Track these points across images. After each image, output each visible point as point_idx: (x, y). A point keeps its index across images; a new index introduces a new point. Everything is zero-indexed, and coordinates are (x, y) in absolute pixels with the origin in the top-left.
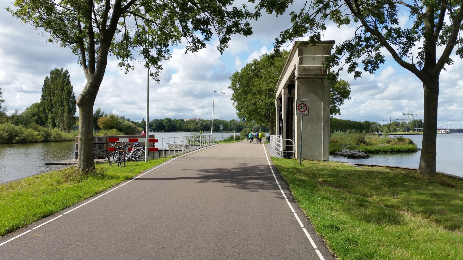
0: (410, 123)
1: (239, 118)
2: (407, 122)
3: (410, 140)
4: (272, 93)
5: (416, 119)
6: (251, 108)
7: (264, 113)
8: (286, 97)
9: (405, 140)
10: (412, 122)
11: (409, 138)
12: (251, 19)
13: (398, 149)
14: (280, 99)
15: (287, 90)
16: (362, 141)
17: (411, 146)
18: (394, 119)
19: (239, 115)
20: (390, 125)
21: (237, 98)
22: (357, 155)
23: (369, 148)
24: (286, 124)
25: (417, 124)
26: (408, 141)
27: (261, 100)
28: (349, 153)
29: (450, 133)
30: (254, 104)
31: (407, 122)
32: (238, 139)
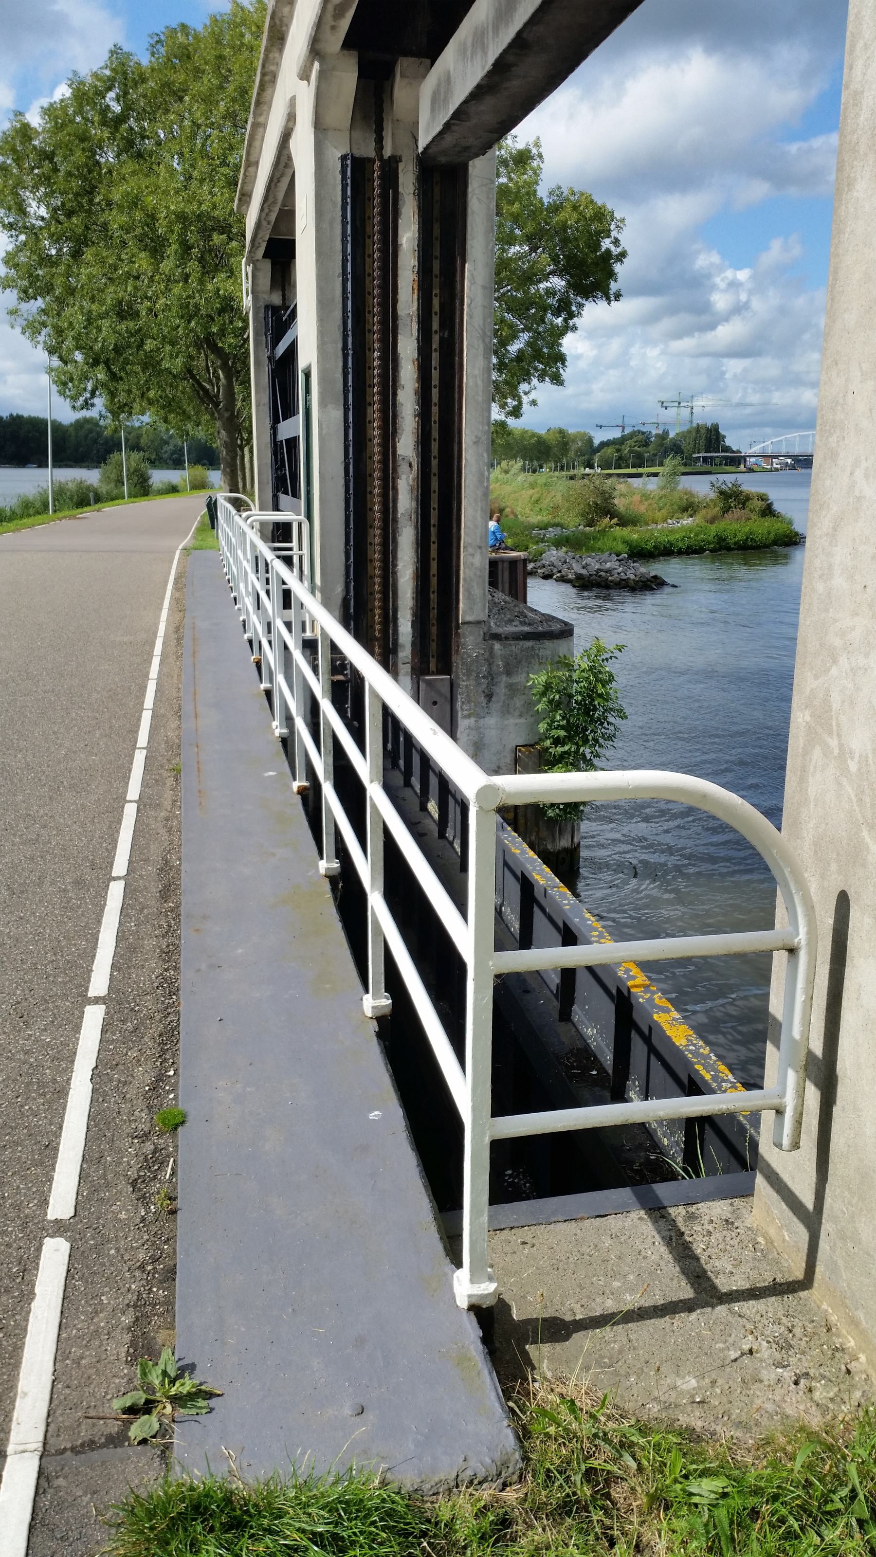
0: (683, 435)
1: (62, 393)
2: (672, 435)
3: (763, 498)
4: (217, 239)
5: (700, 422)
6: (107, 333)
7: (179, 361)
8: (334, 154)
9: (748, 498)
10: (689, 432)
11: (762, 490)
12: (147, 49)
13: (740, 537)
14: (280, 253)
15: (347, 79)
16: (603, 508)
17: (761, 528)
18: (634, 422)
19: (63, 383)
20: (621, 441)
21: (33, 279)
22: (615, 577)
23: (633, 534)
24: (337, 414)
25: (703, 442)
26: (758, 504)
27: (166, 292)
28: (577, 568)
29: (793, 468)
30: (124, 311)
31: (672, 435)
32: (84, 499)
